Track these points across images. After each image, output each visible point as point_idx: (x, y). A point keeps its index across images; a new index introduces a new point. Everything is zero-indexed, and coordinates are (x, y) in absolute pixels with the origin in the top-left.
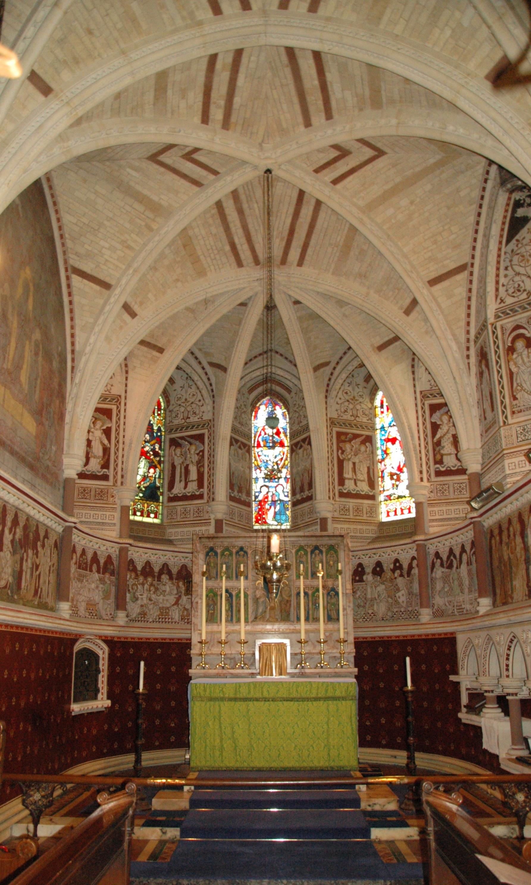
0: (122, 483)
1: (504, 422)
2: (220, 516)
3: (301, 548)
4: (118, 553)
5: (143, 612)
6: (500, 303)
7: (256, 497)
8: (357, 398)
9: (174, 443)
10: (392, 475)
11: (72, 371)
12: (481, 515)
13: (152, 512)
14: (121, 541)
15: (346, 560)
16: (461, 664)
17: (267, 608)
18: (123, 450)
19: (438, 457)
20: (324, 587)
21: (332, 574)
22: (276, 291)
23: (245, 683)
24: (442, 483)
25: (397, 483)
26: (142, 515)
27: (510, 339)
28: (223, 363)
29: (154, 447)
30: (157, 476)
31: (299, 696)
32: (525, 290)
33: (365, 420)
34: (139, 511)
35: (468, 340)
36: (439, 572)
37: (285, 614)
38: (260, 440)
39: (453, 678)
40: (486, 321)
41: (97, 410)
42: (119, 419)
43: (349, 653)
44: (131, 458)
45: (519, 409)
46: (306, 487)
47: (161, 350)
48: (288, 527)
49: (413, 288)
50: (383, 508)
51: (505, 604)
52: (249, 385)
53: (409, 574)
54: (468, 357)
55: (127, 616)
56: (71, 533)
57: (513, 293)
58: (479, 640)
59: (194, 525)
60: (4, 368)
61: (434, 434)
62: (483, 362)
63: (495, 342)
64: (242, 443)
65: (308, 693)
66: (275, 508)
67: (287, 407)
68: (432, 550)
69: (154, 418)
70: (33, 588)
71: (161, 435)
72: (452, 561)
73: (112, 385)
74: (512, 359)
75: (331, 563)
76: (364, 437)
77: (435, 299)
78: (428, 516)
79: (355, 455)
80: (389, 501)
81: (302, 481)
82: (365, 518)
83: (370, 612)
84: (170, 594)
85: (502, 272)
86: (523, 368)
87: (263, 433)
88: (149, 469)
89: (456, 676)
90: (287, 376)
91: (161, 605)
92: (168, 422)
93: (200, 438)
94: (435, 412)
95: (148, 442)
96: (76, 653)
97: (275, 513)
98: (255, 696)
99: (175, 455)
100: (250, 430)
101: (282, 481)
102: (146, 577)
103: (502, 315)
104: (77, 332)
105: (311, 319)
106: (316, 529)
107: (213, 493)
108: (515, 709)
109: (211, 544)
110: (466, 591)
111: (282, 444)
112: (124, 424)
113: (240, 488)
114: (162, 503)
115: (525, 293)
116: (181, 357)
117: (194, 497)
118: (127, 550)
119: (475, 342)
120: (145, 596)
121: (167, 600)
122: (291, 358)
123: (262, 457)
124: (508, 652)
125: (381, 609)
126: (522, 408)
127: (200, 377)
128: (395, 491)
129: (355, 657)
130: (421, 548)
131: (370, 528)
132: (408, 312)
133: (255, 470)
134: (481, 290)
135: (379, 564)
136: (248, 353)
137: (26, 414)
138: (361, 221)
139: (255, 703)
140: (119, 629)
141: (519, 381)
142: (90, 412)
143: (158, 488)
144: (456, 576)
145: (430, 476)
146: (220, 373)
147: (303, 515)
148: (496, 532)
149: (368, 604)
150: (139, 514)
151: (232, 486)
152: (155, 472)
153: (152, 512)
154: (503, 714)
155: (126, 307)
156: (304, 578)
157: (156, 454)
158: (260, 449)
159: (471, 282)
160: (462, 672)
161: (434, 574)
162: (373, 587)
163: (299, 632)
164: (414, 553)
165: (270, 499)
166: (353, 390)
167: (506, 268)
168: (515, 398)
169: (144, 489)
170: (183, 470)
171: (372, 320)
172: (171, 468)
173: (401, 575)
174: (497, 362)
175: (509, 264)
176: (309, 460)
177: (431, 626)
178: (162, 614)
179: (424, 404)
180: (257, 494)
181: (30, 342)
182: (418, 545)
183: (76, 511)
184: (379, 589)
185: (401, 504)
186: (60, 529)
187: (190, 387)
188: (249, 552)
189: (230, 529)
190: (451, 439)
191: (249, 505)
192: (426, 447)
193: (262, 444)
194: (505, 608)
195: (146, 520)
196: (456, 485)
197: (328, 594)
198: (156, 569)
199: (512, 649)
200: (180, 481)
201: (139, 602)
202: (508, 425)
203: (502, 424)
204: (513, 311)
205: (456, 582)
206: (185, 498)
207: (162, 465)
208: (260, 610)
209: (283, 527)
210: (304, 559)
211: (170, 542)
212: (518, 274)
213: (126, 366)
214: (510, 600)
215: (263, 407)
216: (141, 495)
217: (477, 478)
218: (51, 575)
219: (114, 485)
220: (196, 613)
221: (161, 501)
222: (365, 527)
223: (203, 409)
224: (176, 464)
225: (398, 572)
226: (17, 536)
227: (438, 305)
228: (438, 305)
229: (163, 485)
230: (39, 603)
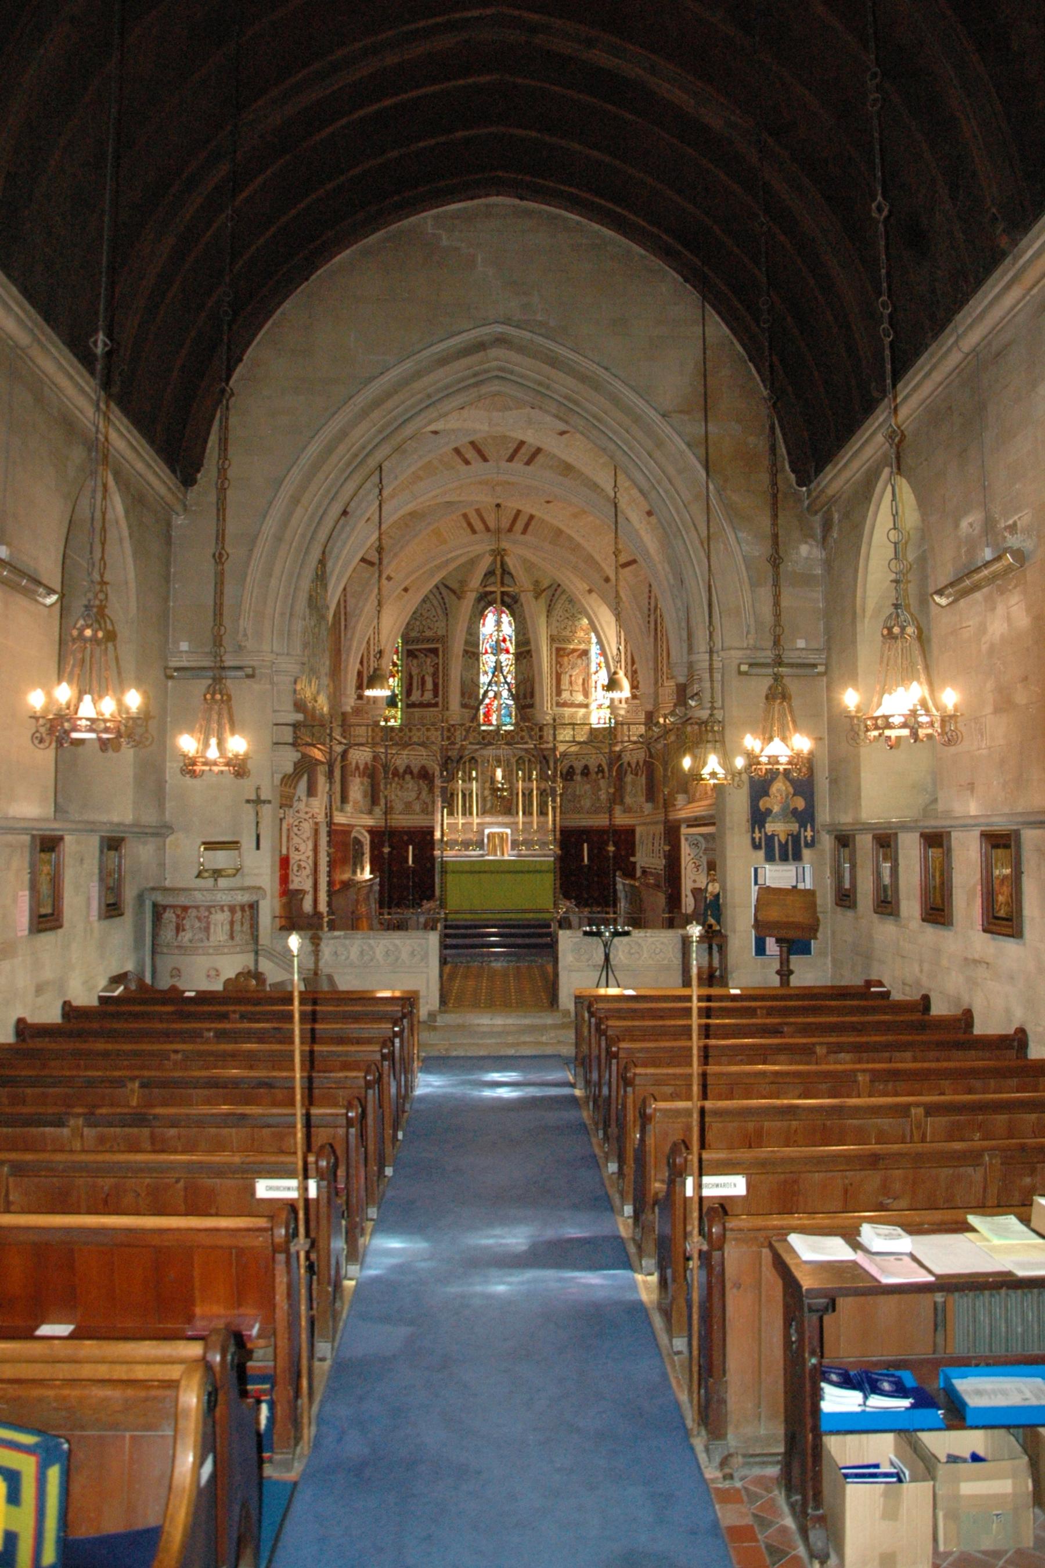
19: (635, 683)
20: (537, 789)
35: (649, 610)
37: (507, 808)
39: (632, 859)
46: (528, 696)
67: (513, 615)
81: (525, 690)
84: (412, 790)
93: (435, 651)
111: (507, 652)
117: (429, 705)
125: (587, 803)
135: (586, 767)
151: (463, 694)
160: (638, 854)
173: (603, 777)
197: (541, 794)
198: (401, 771)
206: (422, 705)
215: (490, 615)
223: (437, 625)
225: (600, 775)
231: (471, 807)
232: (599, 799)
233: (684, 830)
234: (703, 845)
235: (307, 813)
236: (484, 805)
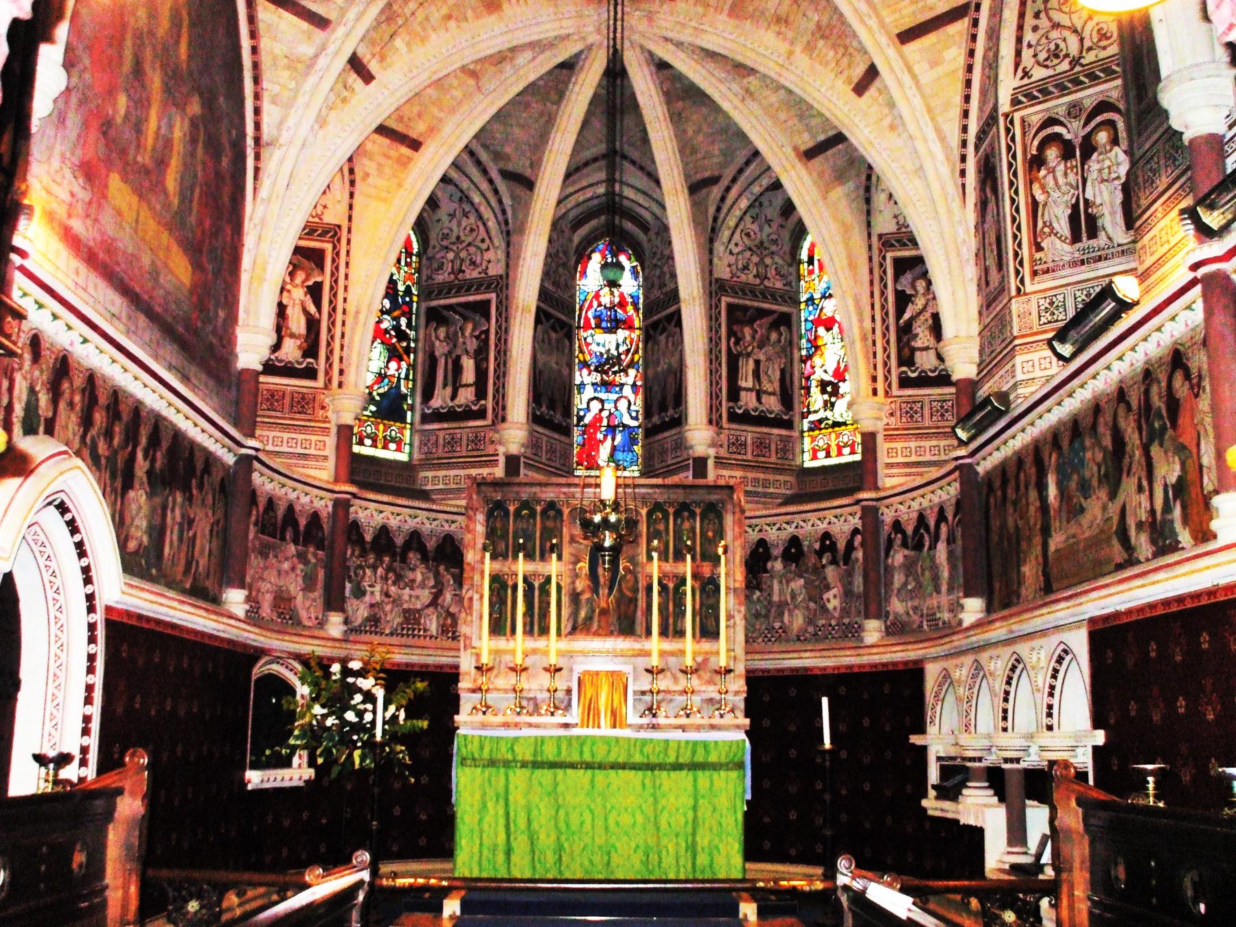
0: (340, 385)
1: (1019, 290)
2: (514, 449)
3: (657, 507)
4: (330, 509)
5: (375, 614)
6: (1022, 78)
7: (580, 419)
8: (766, 244)
9: (436, 317)
10: (823, 385)
11: (256, 178)
12: (973, 454)
13: (393, 440)
14: (337, 488)
15: (737, 529)
16: (929, 713)
17: (594, 611)
18: (344, 323)
20: (695, 576)
22: (627, 44)
23: (551, 737)
24: (911, 399)
25: (833, 399)
27: (1036, 143)
28: (528, 173)
29: (398, 323)
30: (403, 376)
31: (645, 761)
32: (1067, 56)
33: (779, 285)
34: (368, 436)
35: (964, 144)
36: (898, 557)
37: (626, 622)
38: (590, 314)
39: (915, 739)
40: (995, 108)
41: (298, 250)
42: (337, 268)
43: (737, 693)
44: (357, 339)
45: (1045, 266)
47: (415, 145)
51: (1006, 605)
52: (572, 215)
54: (963, 173)
55: (346, 622)
56: (250, 470)
57: (1046, 60)
58: (962, 670)
59: (465, 465)
60: (137, 163)
61: (900, 312)
62: (989, 183)
63: (1009, 148)
64: (557, 317)
65: (662, 756)
66: (613, 439)
67: (640, 258)
68: (888, 516)
69: (399, 269)
70: (183, 562)
71: (411, 301)
72: (922, 536)
73: (325, 207)
74: (1037, 179)
75: (710, 534)
76: (775, 316)
78: (882, 458)
79: (760, 347)
80: (817, 432)
82: (773, 459)
83: (777, 625)
84: (423, 585)
85: (1029, 21)
86: (1055, 195)
87: (595, 304)
88: (388, 362)
89: (921, 736)
90: (640, 199)
91: (405, 606)
92: (424, 278)
93: (482, 309)
94: (905, 272)
95: (388, 312)
96: (256, 681)
97: (614, 449)
98: (568, 759)
99: (437, 338)
100: (573, 296)
101: (627, 391)
102: (379, 559)
103: (1024, 99)
104: (266, 106)
105: (683, 95)
106: (687, 477)
107: (504, 408)
108: (1014, 787)
110: (944, 588)
112: (347, 276)
113: (552, 400)
114: (411, 424)
115: (1067, 60)
116: (449, 160)
119: (977, 148)
120: (378, 588)
121: (418, 597)
122: (650, 169)
123: (594, 347)
124: (1007, 688)
125: (797, 621)
126: (1051, 265)
127: (485, 198)
128: (828, 414)
129: (746, 700)
130: (870, 514)
132: (860, 88)
133: (580, 370)
134: (991, 54)
135: (794, 541)
136: (572, 156)
137: (175, 248)
139: (569, 771)
140: (330, 644)
141: (1046, 218)
142: (285, 254)
143: (405, 396)
144: (928, 563)
145: (890, 386)
146: (520, 190)
147: (663, 452)
148: (997, 483)
149: (773, 611)
150: (368, 442)
152: (399, 368)
153: (393, 440)
154: (996, 798)
155: (356, 64)
156: (660, 559)
157: (402, 336)
158: (590, 331)
159: (974, 38)
160: (932, 730)
161: (890, 561)
162: (786, 586)
164: (856, 522)
165: (605, 423)
166: (761, 230)
167: (1037, 15)
168: (1039, 248)
169: (378, 398)
170: (450, 366)
171: (801, 109)
172: (427, 362)
173: (834, 562)
174: (1011, 184)
175: (1042, 7)
176: (677, 357)
177: (881, 650)
178: (407, 620)
179: (884, 258)
180: (582, 413)
181: (183, 120)
182: (864, 509)
183: (258, 432)
184: (793, 585)
185: (838, 437)
186: (230, 459)
187: (466, 215)
188: (566, 511)
189: (530, 473)
190: (930, 321)
191: (567, 432)
192: (884, 335)
193: (593, 323)
194: (1005, 612)
196: (935, 404)
198: (399, 541)
199: (1014, 682)
200: (445, 386)
201: (367, 598)
202: (1025, 294)
203: (1013, 293)
204: (1045, 92)
205: (927, 573)
207: (412, 356)
208: (583, 614)
210: (661, 527)
211: (425, 495)
212: (1056, 26)
213: (351, 171)
214: (1015, 601)
216: (373, 408)
217: (970, 386)
218: (214, 539)
219: (326, 387)
220: (469, 618)
221: (409, 420)
222: (771, 477)
223: (487, 256)
224: (437, 354)
226: (158, 464)
228: (914, 77)
229: (413, 390)
230: (193, 586)
231: (545, 614)
232: (824, 608)
236: (575, 614)
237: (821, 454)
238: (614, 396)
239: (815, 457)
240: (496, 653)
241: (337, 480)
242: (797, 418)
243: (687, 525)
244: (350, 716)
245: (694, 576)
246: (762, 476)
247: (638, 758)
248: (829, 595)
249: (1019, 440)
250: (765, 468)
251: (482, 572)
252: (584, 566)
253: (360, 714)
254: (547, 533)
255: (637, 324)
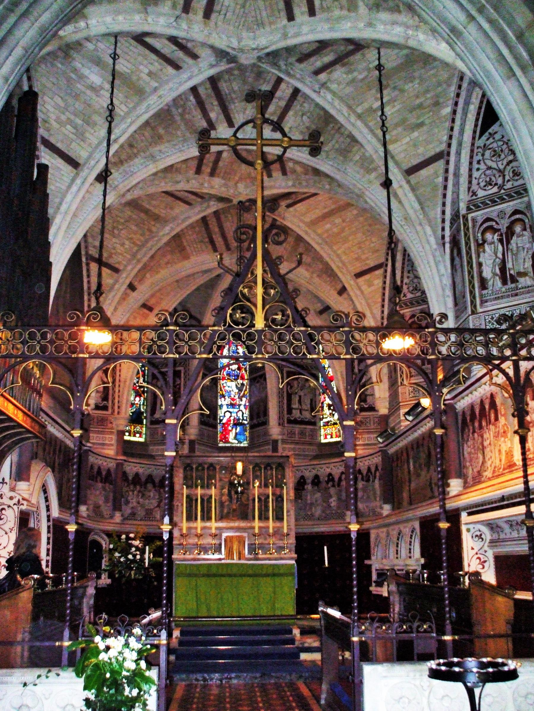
0: (118, 413)
2: (193, 437)
7: (221, 420)
13: (138, 432)
20: (273, 494)
21: (279, 485)
26: (130, 435)
37: (244, 514)
39: (367, 562)
40: (458, 211)
46: (261, 414)
48: (246, 445)
49: (343, 279)
50: (323, 432)
51: (399, 508)
53: (339, 485)
77: (359, 288)
84: (154, 498)
97: (236, 434)
101: (242, 408)
102: (135, 486)
109: (188, 461)
118: (122, 464)
120: (134, 500)
123: (227, 388)
125: (318, 512)
128: (332, 419)
131: (312, 447)
135: (317, 477)
138: (307, 233)
143: (143, 413)
147: (259, 436)
153: (138, 432)
160: (373, 558)
162: (312, 495)
163: (254, 528)
164: (342, 469)
173: (333, 486)
175: (481, 158)
178: (147, 514)
191: (215, 427)
195: (132, 439)
198: (143, 479)
201: (131, 505)
204: (412, 304)
209: (242, 445)
222: (307, 447)
227: (362, 292)
228: (362, 292)
232: (329, 506)
233: (464, 517)
234: (488, 535)
235: (11, 498)
236: (222, 511)
237: (329, 437)
238: (236, 410)
239: (326, 438)
240: (189, 529)
241: (117, 454)
242: (318, 420)
243: (269, 472)
244: (130, 557)
245: (273, 494)
246: (302, 447)
247: (250, 572)
248: (331, 500)
249: (402, 443)
250: (303, 443)
251: (183, 494)
252: (226, 491)
253: (135, 556)
254: (210, 478)
255: (246, 377)
